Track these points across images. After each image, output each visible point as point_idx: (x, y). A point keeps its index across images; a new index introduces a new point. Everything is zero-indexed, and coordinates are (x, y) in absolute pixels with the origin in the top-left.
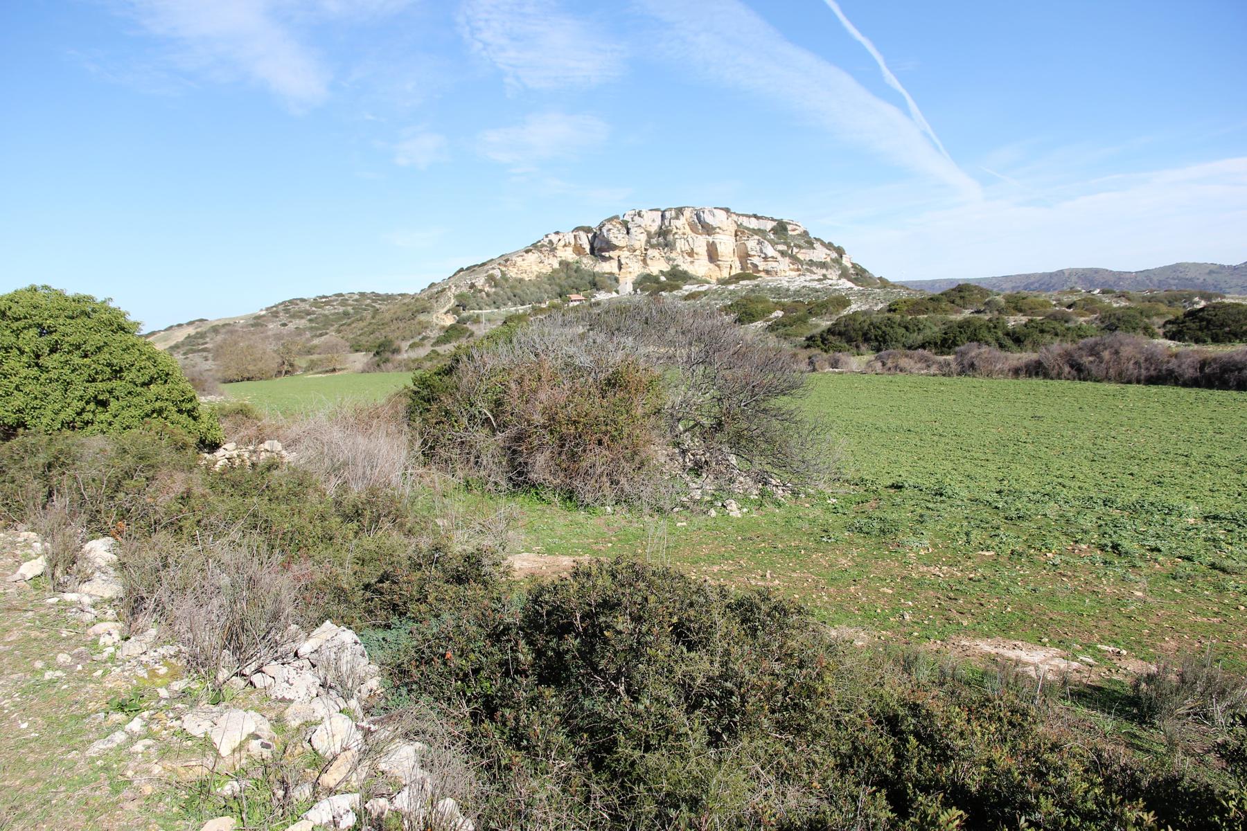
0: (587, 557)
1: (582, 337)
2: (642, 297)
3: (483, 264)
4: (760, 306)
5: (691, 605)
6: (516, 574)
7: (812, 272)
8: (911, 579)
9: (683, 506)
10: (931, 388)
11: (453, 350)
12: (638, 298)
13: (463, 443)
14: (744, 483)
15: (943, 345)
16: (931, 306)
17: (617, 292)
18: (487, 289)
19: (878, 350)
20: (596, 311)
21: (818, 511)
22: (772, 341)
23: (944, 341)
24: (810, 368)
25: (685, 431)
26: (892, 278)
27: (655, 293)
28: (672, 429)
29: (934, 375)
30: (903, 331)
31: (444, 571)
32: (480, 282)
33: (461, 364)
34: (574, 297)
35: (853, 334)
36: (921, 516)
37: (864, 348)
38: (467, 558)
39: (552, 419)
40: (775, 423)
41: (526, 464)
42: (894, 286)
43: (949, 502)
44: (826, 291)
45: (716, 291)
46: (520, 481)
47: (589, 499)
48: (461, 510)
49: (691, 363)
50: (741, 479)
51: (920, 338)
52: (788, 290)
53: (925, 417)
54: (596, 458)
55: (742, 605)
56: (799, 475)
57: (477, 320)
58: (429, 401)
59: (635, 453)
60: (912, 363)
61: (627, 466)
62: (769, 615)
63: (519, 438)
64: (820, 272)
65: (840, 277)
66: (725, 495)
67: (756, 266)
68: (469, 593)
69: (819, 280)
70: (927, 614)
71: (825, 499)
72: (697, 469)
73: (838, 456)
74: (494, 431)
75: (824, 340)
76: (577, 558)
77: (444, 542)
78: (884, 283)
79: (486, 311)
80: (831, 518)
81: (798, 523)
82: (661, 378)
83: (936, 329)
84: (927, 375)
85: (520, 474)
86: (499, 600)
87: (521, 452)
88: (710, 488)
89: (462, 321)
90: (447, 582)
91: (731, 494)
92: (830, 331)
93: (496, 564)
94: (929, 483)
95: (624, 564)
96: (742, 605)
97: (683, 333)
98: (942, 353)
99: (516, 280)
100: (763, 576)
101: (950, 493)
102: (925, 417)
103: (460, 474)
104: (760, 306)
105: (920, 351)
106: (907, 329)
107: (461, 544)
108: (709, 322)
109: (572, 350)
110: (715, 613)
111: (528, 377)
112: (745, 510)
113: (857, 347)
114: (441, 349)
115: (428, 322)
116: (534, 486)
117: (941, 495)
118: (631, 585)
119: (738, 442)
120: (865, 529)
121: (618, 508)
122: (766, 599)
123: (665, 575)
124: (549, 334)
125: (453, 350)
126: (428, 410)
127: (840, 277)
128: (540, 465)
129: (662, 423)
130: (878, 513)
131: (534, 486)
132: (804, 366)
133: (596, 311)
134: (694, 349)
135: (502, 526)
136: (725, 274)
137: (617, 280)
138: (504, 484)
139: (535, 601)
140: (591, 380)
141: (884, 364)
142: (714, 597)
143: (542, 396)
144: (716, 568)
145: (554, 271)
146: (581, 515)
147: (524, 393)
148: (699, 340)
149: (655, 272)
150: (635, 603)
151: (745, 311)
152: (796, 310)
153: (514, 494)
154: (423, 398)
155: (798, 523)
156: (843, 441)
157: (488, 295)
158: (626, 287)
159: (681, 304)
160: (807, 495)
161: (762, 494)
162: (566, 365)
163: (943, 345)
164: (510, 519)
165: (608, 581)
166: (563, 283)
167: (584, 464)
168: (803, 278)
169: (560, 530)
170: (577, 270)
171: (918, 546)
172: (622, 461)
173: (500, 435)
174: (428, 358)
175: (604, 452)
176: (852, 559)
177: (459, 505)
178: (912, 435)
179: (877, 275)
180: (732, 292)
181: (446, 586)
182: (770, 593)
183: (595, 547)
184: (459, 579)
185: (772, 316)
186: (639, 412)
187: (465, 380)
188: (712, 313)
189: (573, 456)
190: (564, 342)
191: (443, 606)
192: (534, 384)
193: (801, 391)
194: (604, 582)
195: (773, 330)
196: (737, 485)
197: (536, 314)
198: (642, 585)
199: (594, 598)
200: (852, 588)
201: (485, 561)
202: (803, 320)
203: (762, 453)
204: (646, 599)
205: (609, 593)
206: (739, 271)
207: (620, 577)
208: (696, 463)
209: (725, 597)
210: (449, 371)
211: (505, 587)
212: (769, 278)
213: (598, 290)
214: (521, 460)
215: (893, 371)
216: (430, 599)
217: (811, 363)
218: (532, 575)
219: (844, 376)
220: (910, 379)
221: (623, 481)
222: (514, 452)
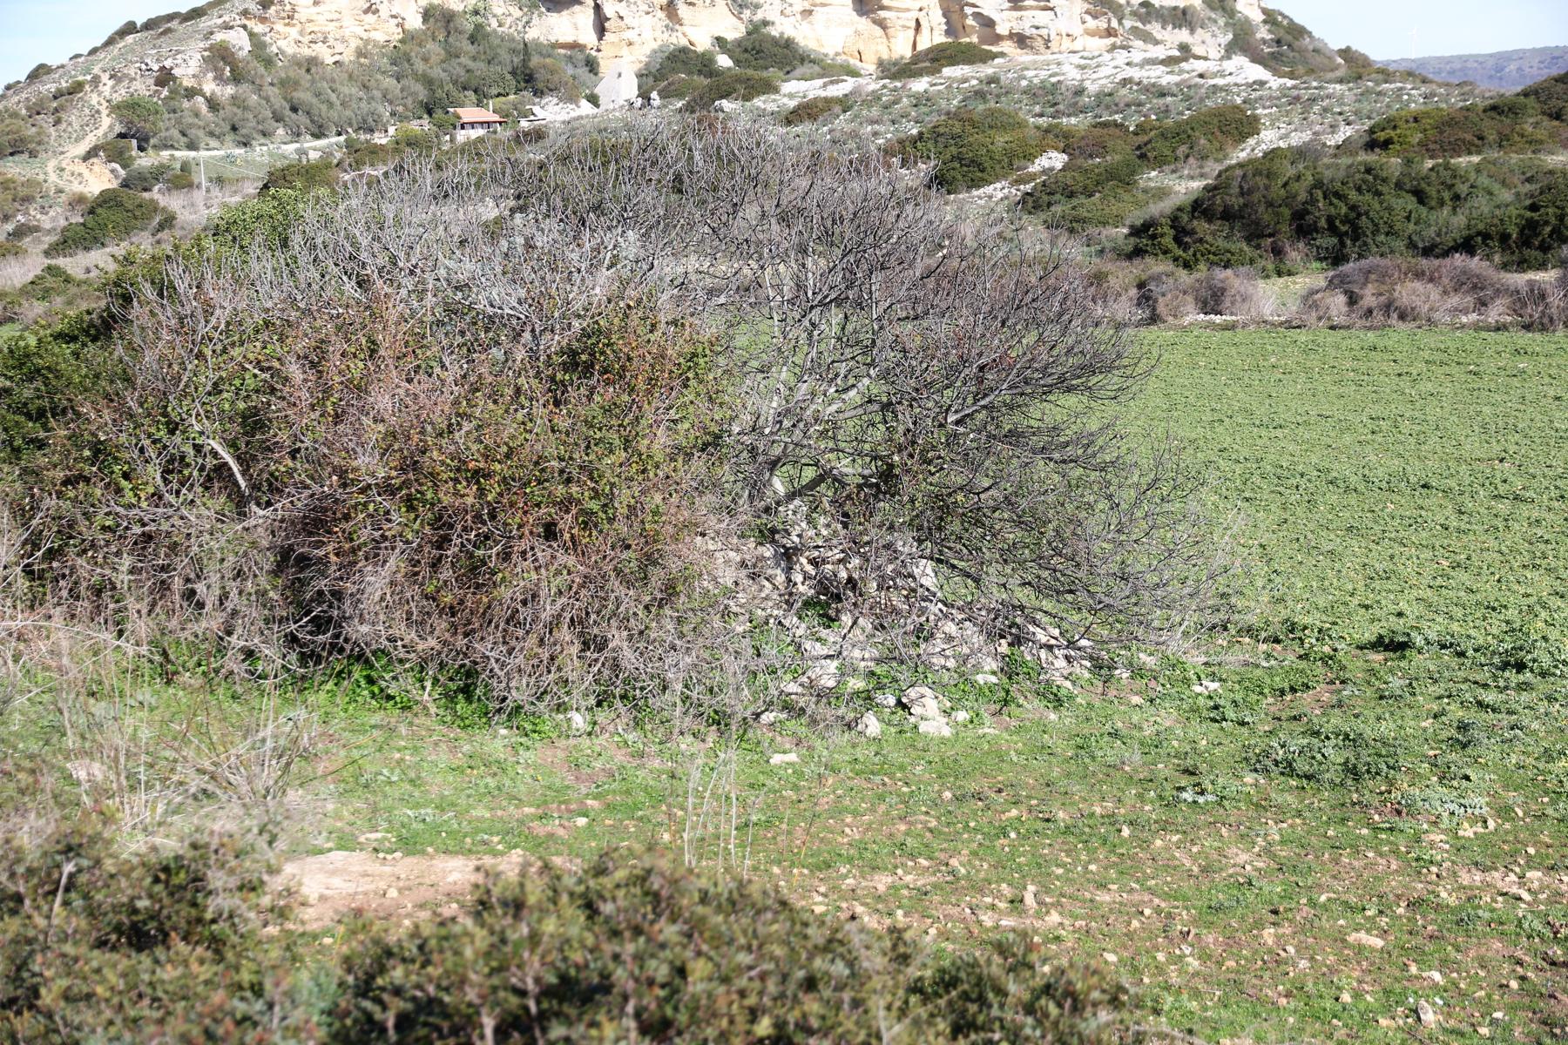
0: (517, 856)
1: (494, 230)
2: (664, 115)
3: (196, 13)
4: (1001, 140)
5: (810, 984)
6: (308, 914)
7: (1148, 38)
8: (1438, 908)
9: (787, 707)
10: (1489, 365)
11: (112, 267)
12: (651, 118)
13: (148, 537)
14: (959, 641)
15: (1525, 242)
16: (1491, 130)
17: (594, 100)
18: (209, 87)
19: (1337, 259)
20: (532, 154)
21: (1167, 717)
22: (1034, 236)
23: (1530, 229)
24: (1140, 314)
25: (791, 496)
26: (1378, 52)
27: (702, 102)
28: (757, 488)
29: (1499, 328)
30: (1410, 202)
31: (92, 912)
32: (188, 66)
33: (136, 310)
34: (469, 113)
35: (1265, 216)
36: (1463, 727)
37: (1294, 255)
38: (164, 872)
39: (410, 465)
40: (1041, 468)
41: (338, 595)
42: (1386, 74)
43: (1543, 686)
44: (1186, 91)
45: (876, 96)
46: (320, 641)
47: (520, 692)
48: (145, 734)
49: (805, 303)
50: (951, 628)
51: (1457, 222)
52: (1079, 92)
53: (1473, 446)
54: (540, 576)
55: (953, 983)
56: (1114, 614)
57: (181, 180)
58: (41, 415)
59: (650, 560)
60: (1434, 293)
61: (628, 599)
62: (1029, 1009)
63: (317, 522)
64: (1171, 38)
65: (1229, 51)
66: (904, 676)
67: (988, 23)
68: (169, 973)
69: (1169, 61)
70: (1487, 1007)
71: (1186, 681)
72: (827, 602)
73: (1220, 560)
74: (240, 504)
75: (1181, 234)
76: (488, 861)
77: (94, 825)
78: (1356, 66)
79: (209, 155)
80: (1204, 735)
81: (1110, 752)
82: (720, 345)
83: (1506, 196)
84: (1477, 327)
85: (320, 624)
86: (257, 990)
87: (323, 562)
88: (862, 656)
89: (137, 182)
90: (101, 944)
91: (921, 670)
92: (1199, 208)
93: (251, 887)
94: (1484, 633)
95: (620, 875)
96: (953, 983)
97: (784, 219)
98: (1523, 265)
99: (296, 62)
100: (1016, 902)
101: (1546, 661)
102: (1473, 446)
103: (142, 627)
104: (1001, 140)
105: (1459, 259)
106: (1420, 196)
107: (143, 832)
108: (855, 186)
109: (467, 268)
110: (878, 1005)
111: (337, 345)
112: (962, 716)
113: (1278, 252)
114: (75, 264)
115: (30, 183)
116: (361, 658)
117: (1520, 667)
118: (637, 931)
119: (940, 526)
120: (1302, 766)
121: (602, 716)
122: (1021, 966)
123: (735, 903)
124: (398, 221)
125: (112, 267)
126: (41, 445)
127: (1229, 51)
128: (377, 596)
129: (725, 472)
130: (1336, 721)
131: (361, 658)
132: (1125, 308)
133: (532, 154)
134: (816, 264)
135: (268, 775)
136: (902, 49)
137: (592, 66)
138: (272, 653)
139: (365, 988)
140: (520, 354)
141: (1353, 300)
142: (874, 961)
143: (382, 401)
144: (882, 882)
145: (409, 37)
146: (498, 740)
147: (327, 391)
148: (827, 237)
149: (703, 44)
150: (651, 983)
151: (959, 153)
152: (1102, 148)
153: (301, 684)
154: (22, 409)
155: (1110, 752)
156: (1235, 519)
157: (213, 104)
158: (619, 85)
159: (776, 134)
160: (1137, 672)
161: (1010, 669)
162: (451, 310)
163: (1525, 242)
164: (291, 755)
165: (575, 923)
166: (437, 73)
167: (505, 593)
168: (1121, 57)
169: (439, 784)
170: (477, 35)
171: (1454, 813)
172: (614, 583)
173: (259, 515)
174: (37, 289)
175: (562, 558)
176: (1268, 851)
177: (136, 719)
178: (1435, 499)
179: (1335, 44)
180: (920, 100)
181: (98, 957)
182: (1030, 948)
183: (540, 829)
184: (139, 935)
185: (1035, 168)
186: (659, 442)
187: (149, 357)
188: (864, 160)
189: (474, 573)
190: (446, 241)
191: (88, 1016)
192: (357, 368)
193: (1114, 380)
194: (562, 925)
195: (1037, 207)
196: (939, 644)
197: (358, 164)
198: (669, 931)
199: (532, 972)
200: (1269, 935)
201: (217, 879)
202: (1122, 178)
203: (1007, 555)
204: (681, 972)
205: (577, 956)
206: (940, 38)
207: (607, 908)
208: (823, 585)
209: (904, 959)
210: (102, 329)
211: (275, 953)
212: (1024, 57)
213: (539, 93)
214: (322, 584)
215: (1378, 317)
216: (47, 998)
217: (1145, 298)
218: (358, 913)
219: (1240, 335)
220: (1428, 339)
221: (618, 638)
222: (304, 561)
